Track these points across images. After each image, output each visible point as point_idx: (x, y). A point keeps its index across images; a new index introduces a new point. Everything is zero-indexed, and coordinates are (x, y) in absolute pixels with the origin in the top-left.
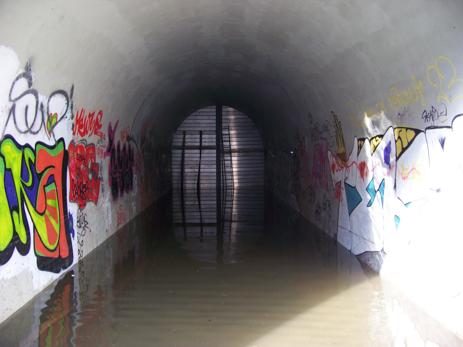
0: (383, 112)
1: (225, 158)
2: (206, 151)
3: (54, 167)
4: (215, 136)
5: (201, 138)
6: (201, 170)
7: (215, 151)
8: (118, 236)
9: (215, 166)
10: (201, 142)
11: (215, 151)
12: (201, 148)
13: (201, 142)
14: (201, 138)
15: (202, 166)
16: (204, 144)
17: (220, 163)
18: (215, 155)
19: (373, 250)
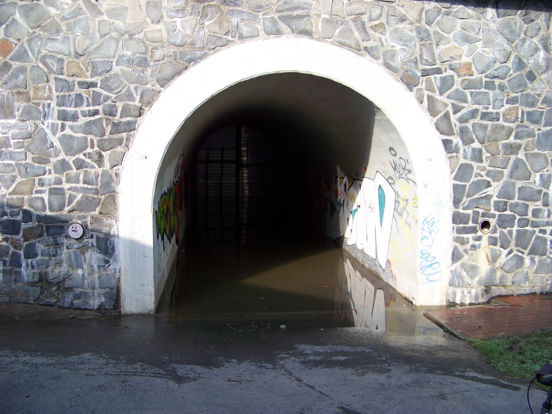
0: (348, 260)
1: (244, 171)
2: (227, 165)
3: (26, 397)
4: (234, 152)
5: (223, 153)
6: (223, 181)
7: (234, 165)
8: (342, 305)
9: (234, 178)
10: (222, 157)
11: (234, 165)
12: (223, 162)
13: (222, 157)
14: (223, 153)
15: (223, 178)
16: (225, 159)
17: (238, 176)
18: (234, 168)
19: (383, 318)
